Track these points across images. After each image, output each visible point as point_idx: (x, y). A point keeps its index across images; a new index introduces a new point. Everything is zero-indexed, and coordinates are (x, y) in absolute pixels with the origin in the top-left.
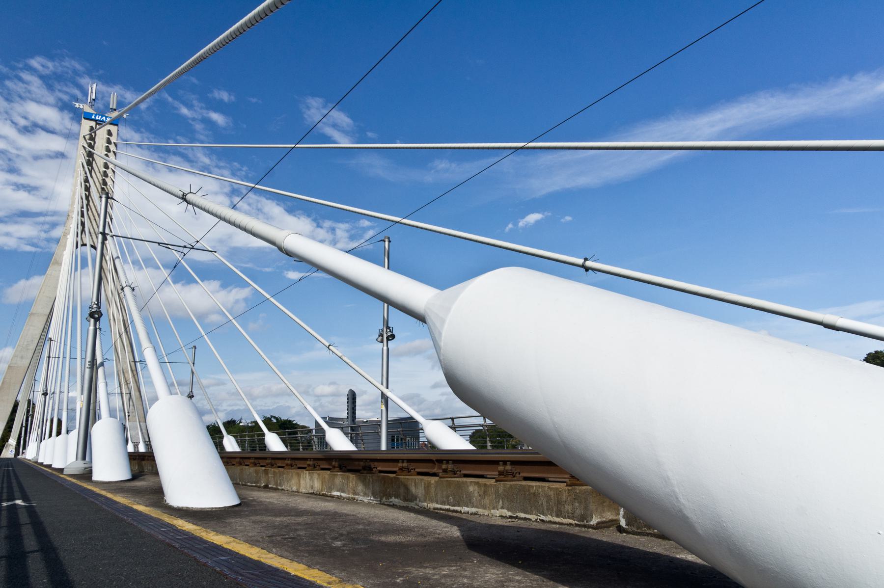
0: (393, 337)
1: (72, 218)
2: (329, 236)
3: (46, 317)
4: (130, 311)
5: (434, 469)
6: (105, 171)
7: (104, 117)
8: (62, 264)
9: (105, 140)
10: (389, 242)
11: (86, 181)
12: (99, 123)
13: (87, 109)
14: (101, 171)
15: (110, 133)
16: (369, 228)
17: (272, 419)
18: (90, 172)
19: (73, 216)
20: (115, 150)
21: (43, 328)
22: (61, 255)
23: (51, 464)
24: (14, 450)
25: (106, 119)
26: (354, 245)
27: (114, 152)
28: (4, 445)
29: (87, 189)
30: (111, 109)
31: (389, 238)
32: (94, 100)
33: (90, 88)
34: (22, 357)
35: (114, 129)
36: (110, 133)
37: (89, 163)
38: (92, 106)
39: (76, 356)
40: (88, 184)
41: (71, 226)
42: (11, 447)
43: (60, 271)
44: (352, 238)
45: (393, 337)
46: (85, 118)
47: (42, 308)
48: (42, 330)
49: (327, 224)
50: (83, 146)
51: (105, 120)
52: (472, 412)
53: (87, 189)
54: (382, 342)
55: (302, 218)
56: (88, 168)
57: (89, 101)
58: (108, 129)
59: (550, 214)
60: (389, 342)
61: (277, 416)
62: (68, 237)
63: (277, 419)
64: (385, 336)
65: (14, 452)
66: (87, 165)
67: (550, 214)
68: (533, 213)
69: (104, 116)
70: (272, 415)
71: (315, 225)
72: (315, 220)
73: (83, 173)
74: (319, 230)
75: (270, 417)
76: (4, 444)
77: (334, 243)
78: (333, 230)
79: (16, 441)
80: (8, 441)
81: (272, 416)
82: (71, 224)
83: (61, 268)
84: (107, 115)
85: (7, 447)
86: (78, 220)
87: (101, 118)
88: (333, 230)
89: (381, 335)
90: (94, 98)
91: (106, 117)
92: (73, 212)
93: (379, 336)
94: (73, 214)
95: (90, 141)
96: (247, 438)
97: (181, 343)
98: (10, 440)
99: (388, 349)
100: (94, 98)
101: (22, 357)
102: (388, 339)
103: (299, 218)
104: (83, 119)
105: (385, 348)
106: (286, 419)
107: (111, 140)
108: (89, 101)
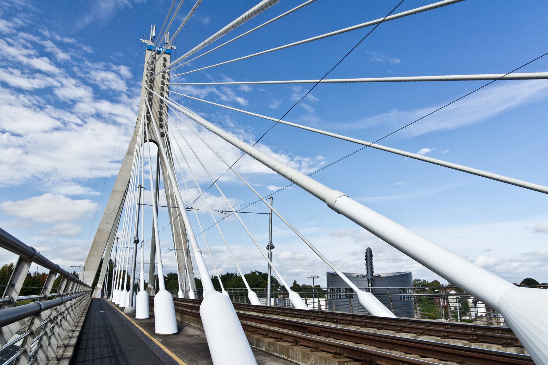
0: (273, 247)
1: (141, 121)
2: (298, 165)
3: (124, 193)
4: (178, 205)
5: (406, 330)
6: (160, 117)
7: (161, 49)
8: (134, 154)
9: (162, 65)
10: (272, 199)
11: (148, 112)
12: (159, 53)
13: (150, 43)
14: (160, 87)
15: (165, 60)
16: (322, 160)
17: (256, 273)
18: (151, 106)
19: (141, 119)
20: (167, 90)
21: (121, 201)
22: (133, 147)
23: (124, 306)
24: (101, 292)
25: (162, 50)
26: (312, 170)
27: (167, 85)
28: (95, 288)
29: (149, 118)
30: (166, 43)
31: (272, 197)
32: (154, 36)
33: (151, 29)
34: (107, 223)
35: (168, 57)
36: (165, 60)
37: (150, 100)
38: (153, 41)
39: (152, 204)
40: (149, 115)
41: (140, 126)
42: (99, 290)
43: (133, 159)
44: (310, 166)
45: (273, 247)
46: (148, 49)
47: (120, 187)
48: (120, 203)
49: (297, 158)
50: (145, 88)
51: (162, 50)
52: (29, 317)
53: (149, 118)
54: (268, 249)
55: (283, 155)
56: (149, 103)
57: (151, 38)
58: (164, 56)
59: (435, 149)
60: (272, 250)
61: (259, 271)
62: (138, 134)
63: (259, 273)
64: (270, 246)
65: (101, 294)
66: (148, 101)
67: (435, 149)
68: (424, 148)
69: (161, 48)
70: (256, 270)
71: (290, 159)
72: (290, 156)
73: (146, 108)
74: (292, 162)
75: (254, 271)
76: (94, 287)
77: (299, 169)
78: (300, 162)
79: (102, 286)
80: (96, 285)
81: (256, 271)
82: (140, 125)
83: (133, 157)
84: (163, 47)
85: (96, 289)
86: (145, 122)
87: (159, 49)
88: (300, 162)
89: (268, 246)
90: (154, 35)
91: (163, 49)
92: (141, 116)
93: (267, 246)
94: (141, 118)
95: (151, 71)
96: (238, 292)
97: (203, 234)
98: (98, 285)
99: (271, 253)
100: (154, 35)
101: (107, 223)
102: (271, 248)
103: (280, 155)
104: (147, 50)
105: (270, 252)
106: (265, 273)
107: (166, 64)
108: (151, 38)
